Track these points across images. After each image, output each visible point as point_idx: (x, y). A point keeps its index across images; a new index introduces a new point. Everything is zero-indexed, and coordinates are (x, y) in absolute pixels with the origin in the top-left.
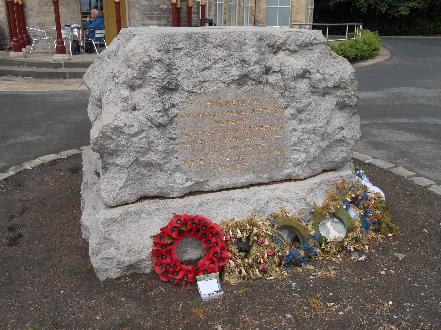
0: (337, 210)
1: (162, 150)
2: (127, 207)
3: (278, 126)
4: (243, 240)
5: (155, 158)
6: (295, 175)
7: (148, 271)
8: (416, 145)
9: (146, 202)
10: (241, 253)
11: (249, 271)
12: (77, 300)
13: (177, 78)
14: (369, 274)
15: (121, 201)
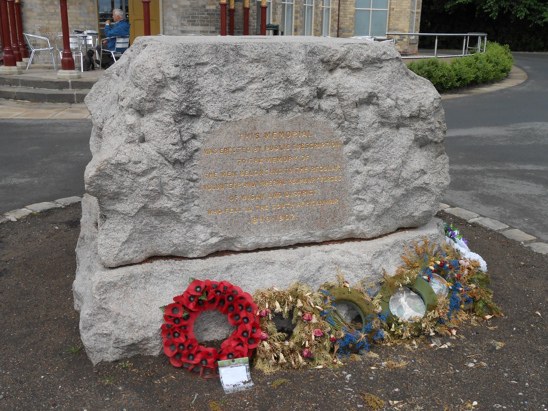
0: (414, 281)
1: (178, 194)
2: (131, 268)
3: (335, 167)
4: (284, 316)
5: (169, 204)
6: (359, 232)
7: (156, 353)
8: (542, 200)
9: (157, 263)
10: (280, 333)
11: (290, 357)
12: (60, 387)
13: (200, 101)
14: (452, 367)
15: (123, 260)
